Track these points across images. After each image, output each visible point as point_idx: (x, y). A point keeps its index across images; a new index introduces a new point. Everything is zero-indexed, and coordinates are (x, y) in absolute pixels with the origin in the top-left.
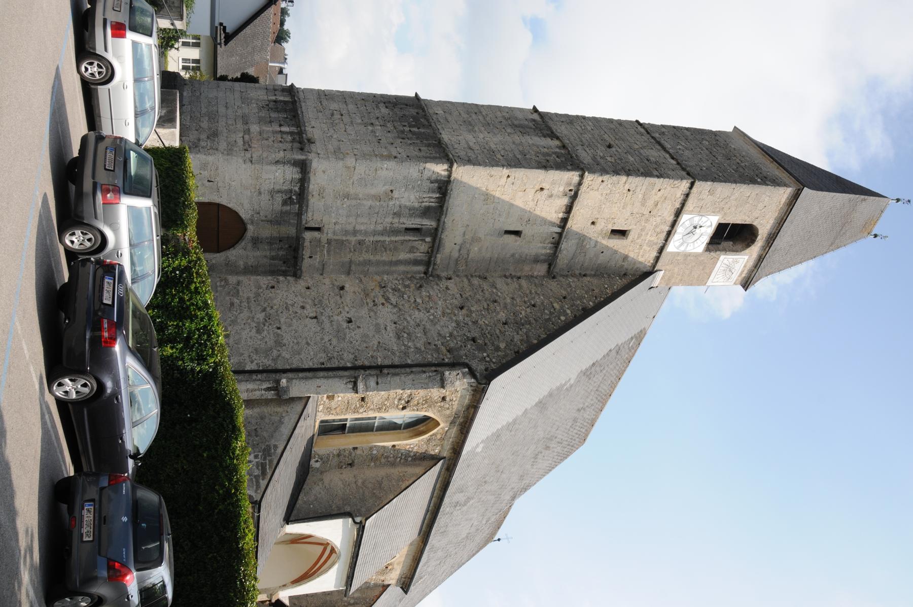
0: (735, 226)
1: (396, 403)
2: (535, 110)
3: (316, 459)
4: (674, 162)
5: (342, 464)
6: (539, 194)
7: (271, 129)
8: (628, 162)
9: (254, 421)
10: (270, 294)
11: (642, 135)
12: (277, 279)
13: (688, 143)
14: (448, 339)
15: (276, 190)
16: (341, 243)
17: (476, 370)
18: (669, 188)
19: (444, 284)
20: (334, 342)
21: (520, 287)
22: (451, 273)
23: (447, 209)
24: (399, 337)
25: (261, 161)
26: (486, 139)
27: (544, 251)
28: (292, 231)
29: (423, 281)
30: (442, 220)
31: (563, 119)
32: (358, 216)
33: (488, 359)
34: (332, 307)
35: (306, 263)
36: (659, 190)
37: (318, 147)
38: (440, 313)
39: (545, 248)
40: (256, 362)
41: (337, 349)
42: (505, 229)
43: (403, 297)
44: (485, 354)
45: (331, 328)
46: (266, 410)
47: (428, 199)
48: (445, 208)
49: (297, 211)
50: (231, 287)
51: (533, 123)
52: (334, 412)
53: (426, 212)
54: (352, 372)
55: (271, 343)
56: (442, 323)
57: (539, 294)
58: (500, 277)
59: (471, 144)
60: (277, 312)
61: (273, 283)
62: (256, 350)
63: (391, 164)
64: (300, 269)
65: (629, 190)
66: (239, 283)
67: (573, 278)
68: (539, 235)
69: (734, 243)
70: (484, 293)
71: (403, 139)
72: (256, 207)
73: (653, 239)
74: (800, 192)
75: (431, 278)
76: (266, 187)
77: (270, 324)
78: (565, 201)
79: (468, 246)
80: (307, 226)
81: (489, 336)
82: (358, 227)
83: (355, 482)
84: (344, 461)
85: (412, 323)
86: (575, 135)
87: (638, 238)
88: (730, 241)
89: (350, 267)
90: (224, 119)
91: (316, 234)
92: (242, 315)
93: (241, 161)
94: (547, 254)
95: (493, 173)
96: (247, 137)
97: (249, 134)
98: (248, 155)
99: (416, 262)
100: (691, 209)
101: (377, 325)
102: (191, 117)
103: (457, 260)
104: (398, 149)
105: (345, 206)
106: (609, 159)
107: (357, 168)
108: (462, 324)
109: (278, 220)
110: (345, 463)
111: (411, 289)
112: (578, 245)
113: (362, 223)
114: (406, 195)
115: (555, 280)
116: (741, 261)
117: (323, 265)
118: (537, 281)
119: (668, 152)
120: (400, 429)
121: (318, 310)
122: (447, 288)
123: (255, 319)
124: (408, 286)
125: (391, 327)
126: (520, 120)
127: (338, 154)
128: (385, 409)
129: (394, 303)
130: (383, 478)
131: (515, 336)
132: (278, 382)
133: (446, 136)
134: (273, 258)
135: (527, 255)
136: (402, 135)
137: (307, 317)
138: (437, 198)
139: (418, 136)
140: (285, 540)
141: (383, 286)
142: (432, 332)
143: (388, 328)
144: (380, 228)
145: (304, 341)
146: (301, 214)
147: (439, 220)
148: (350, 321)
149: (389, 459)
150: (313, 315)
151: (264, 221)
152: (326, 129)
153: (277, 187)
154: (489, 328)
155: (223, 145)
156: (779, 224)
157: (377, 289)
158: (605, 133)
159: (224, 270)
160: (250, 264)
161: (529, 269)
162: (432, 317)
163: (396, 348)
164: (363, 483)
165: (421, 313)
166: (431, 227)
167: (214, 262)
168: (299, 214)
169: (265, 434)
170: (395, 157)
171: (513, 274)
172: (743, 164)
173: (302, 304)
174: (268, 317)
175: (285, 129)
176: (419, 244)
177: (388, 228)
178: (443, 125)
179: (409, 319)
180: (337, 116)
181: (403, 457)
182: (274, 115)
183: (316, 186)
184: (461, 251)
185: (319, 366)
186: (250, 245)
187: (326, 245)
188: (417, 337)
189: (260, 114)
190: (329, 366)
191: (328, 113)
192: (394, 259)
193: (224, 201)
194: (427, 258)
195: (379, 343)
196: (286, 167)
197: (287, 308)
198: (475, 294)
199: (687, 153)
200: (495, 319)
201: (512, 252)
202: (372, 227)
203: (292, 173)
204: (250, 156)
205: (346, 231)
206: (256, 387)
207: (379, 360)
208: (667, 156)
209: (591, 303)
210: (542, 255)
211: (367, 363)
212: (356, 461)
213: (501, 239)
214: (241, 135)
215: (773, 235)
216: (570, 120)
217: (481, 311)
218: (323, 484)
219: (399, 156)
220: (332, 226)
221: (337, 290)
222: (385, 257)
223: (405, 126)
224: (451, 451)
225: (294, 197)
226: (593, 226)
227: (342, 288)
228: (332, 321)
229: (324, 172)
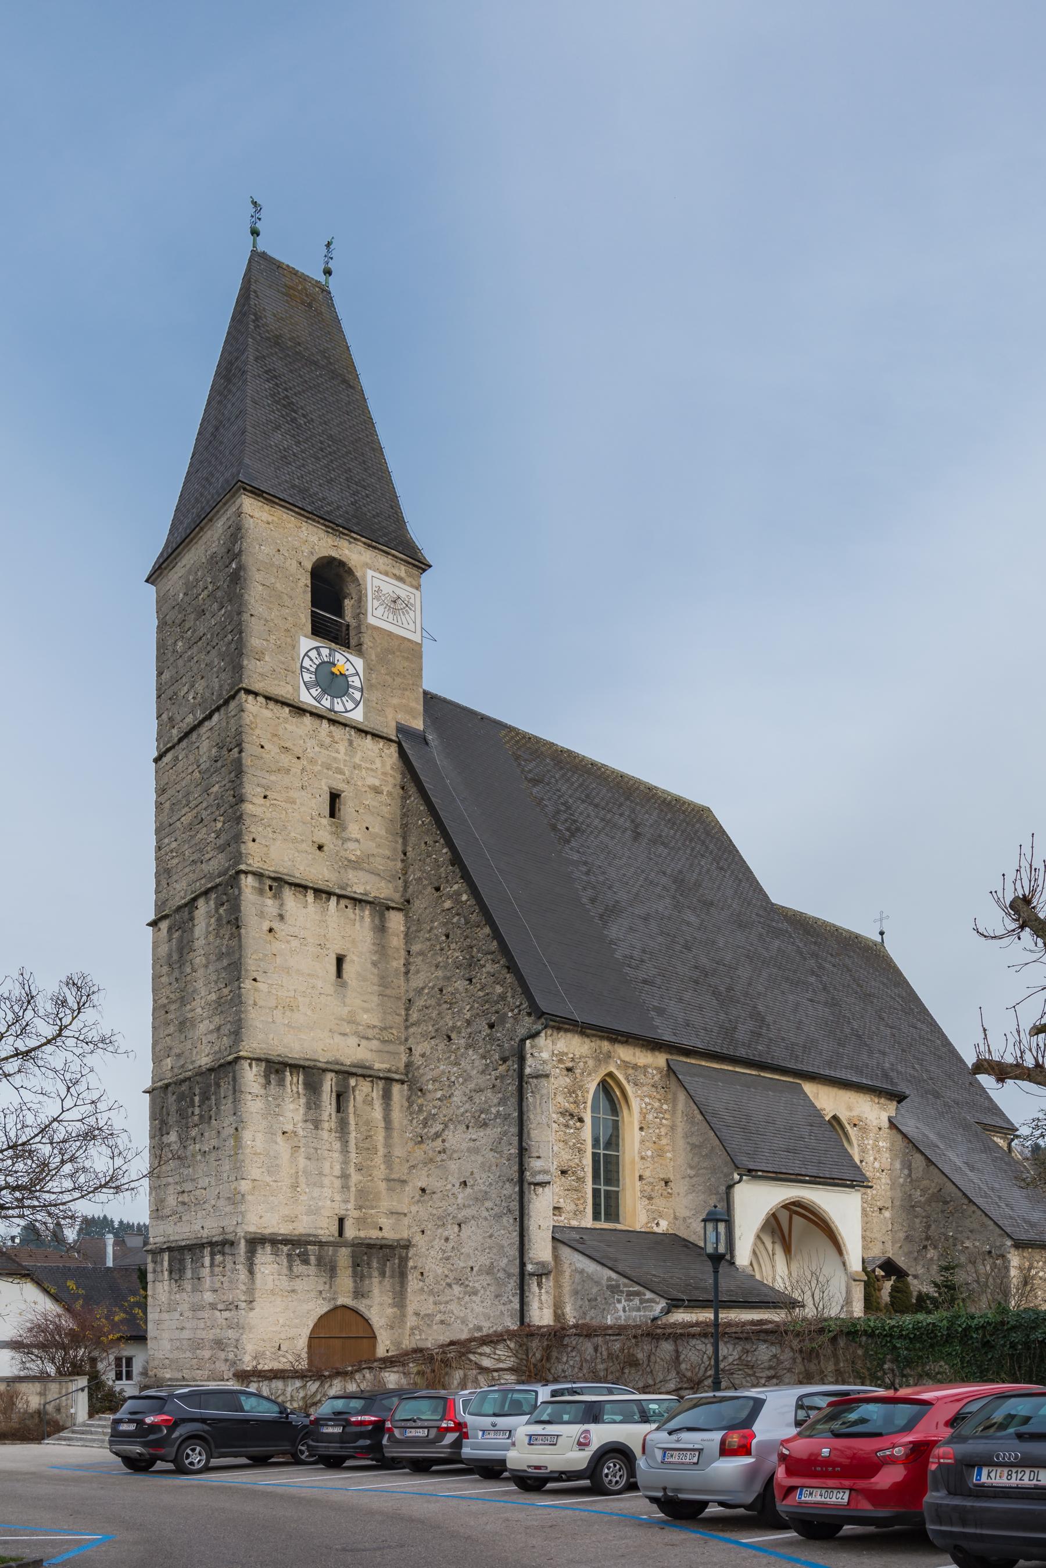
0: (316, 601)
1: (572, 1131)
2: (153, 924)
3: (654, 1225)
4: (216, 717)
5: (665, 1193)
6: (280, 934)
7: (208, 1278)
8: (222, 796)
9: (580, 1303)
10: (430, 1279)
11: (177, 757)
12: (412, 1268)
13: (184, 680)
14: (488, 1061)
15: (288, 1273)
16: (362, 1193)
17: (529, 1029)
18: (257, 732)
19: (418, 1061)
20: (488, 1204)
21: (421, 953)
22: (402, 1048)
23: (308, 1060)
24: (485, 1125)
25: (251, 1291)
26: (203, 1005)
27: (367, 920)
28: (344, 1253)
29: (414, 1087)
30: (324, 1066)
31: (164, 883)
32: (321, 1174)
33: (516, 1011)
34: (447, 1204)
35: (389, 1234)
36: (262, 747)
37: (229, 1223)
38: (455, 1069)
39: (362, 917)
40: (510, 1297)
41: (498, 1202)
42: (334, 978)
43: (434, 1115)
44: (510, 1014)
45: (473, 1207)
46: (567, 1289)
47: (293, 1087)
48: (307, 1063)
49: (317, 1248)
50: (422, 1323)
51: (173, 931)
52: (581, 1207)
53: (313, 1088)
54: (526, 1186)
55: (488, 1279)
56: (469, 1068)
57: (431, 928)
58: (408, 980)
59: (212, 1027)
60: (452, 1271)
61: (417, 1274)
62: (497, 1296)
63: (247, 1136)
64: (398, 1241)
65: (265, 797)
66: (417, 1314)
67: (409, 873)
68: (342, 929)
69: (345, 598)
70: (430, 1006)
71: (210, 1118)
72: (313, 1294)
73: (342, 747)
74: (248, 488)
75: (410, 1076)
76: (284, 1283)
77: (467, 1279)
78: (288, 893)
79: (361, 1027)
80: (337, 1234)
81: (487, 1006)
82: (337, 1172)
83: (691, 1177)
84: (660, 1192)
85: (467, 1106)
86: (187, 870)
87: (342, 773)
88: (344, 603)
89: (394, 1180)
90: (199, 1332)
91: (348, 1224)
92: (455, 1312)
93: (251, 1314)
94: (370, 915)
95: (251, 1002)
96: (220, 1307)
97: (216, 1304)
98: (243, 1305)
99: (387, 1096)
100: (289, 688)
101: (469, 1150)
102: (198, 1369)
103: (384, 1042)
104: (225, 1125)
105: (307, 1190)
106: (219, 825)
107: (252, 1178)
108: (470, 1041)
109: (330, 1269)
110: (664, 1190)
111: (425, 1103)
112: (356, 869)
113: (332, 1168)
114: (289, 1115)
115: (411, 901)
116: (377, 582)
117: (392, 1213)
118: (414, 928)
119: (201, 723)
120: (617, 1121)
121: (450, 1221)
122: (423, 1055)
123: (461, 1296)
124: (421, 1107)
125: (473, 1133)
126: (171, 950)
127: (236, 1199)
128: (581, 1143)
129: (442, 1126)
130: (688, 1143)
131: (487, 969)
132: (532, 1275)
133: (204, 1061)
134: (383, 1274)
135: (374, 944)
136: (206, 1119)
137: (458, 1236)
138: (291, 1075)
139: (205, 1098)
140: (831, 1244)
141: (420, 1139)
142: (480, 1081)
143: (474, 1137)
144: (337, 1145)
145: (489, 1240)
146: (320, 1242)
147: (325, 1070)
148: (465, 1183)
149: (663, 1133)
150: (456, 1229)
151: (331, 1284)
152: (204, 1212)
153: (285, 1271)
154: (476, 1005)
155: (231, 1333)
156: (308, 518)
157: (424, 1146)
158: (179, 820)
159: (400, 1331)
160: (390, 1301)
161: (396, 938)
162: (461, 1080)
163: (499, 1129)
164: (691, 1167)
165: (455, 1093)
166: (334, 1080)
167: (388, 1342)
168: (321, 1244)
169: (595, 1290)
170: (236, 1129)
171: (402, 961)
172: (210, 587)
173: (443, 1241)
174: (459, 1281)
175: (207, 1261)
176: (359, 1094)
177: (337, 1135)
178: (188, 1061)
179: (462, 1110)
180: (185, 1198)
181: (661, 1115)
182: (189, 1274)
183: (280, 1226)
184: (370, 1037)
185: (518, 1224)
186: (365, 1301)
187: (364, 1210)
188: (486, 1102)
189: (189, 1290)
190: (517, 1213)
191: (181, 1209)
192: (382, 1124)
193: (306, 1332)
194: (379, 1082)
195: (491, 1150)
196: (256, 1261)
197: (448, 1258)
198: (430, 1018)
199: (200, 686)
200: (463, 994)
201: (370, 966)
202: (336, 1155)
203: (264, 1258)
204: (245, 1304)
205: (342, 1187)
206: (537, 1299)
207: (512, 1151)
208: (206, 723)
209: (444, 851)
210: (373, 921)
211: (516, 1168)
212: (662, 1176)
213: (350, 982)
214: (218, 1313)
215: (328, 527)
216: (164, 874)
217: (453, 1013)
218: (690, 1218)
219: (234, 1126)
220: (336, 1205)
221: (426, 1198)
222: (380, 1137)
223: (193, 1113)
224: (657, 1053)
225: (298, 1251)
226: (325, 848)
227: (423, 1190)
228: (464, 1206)
229: (261, 1217)
